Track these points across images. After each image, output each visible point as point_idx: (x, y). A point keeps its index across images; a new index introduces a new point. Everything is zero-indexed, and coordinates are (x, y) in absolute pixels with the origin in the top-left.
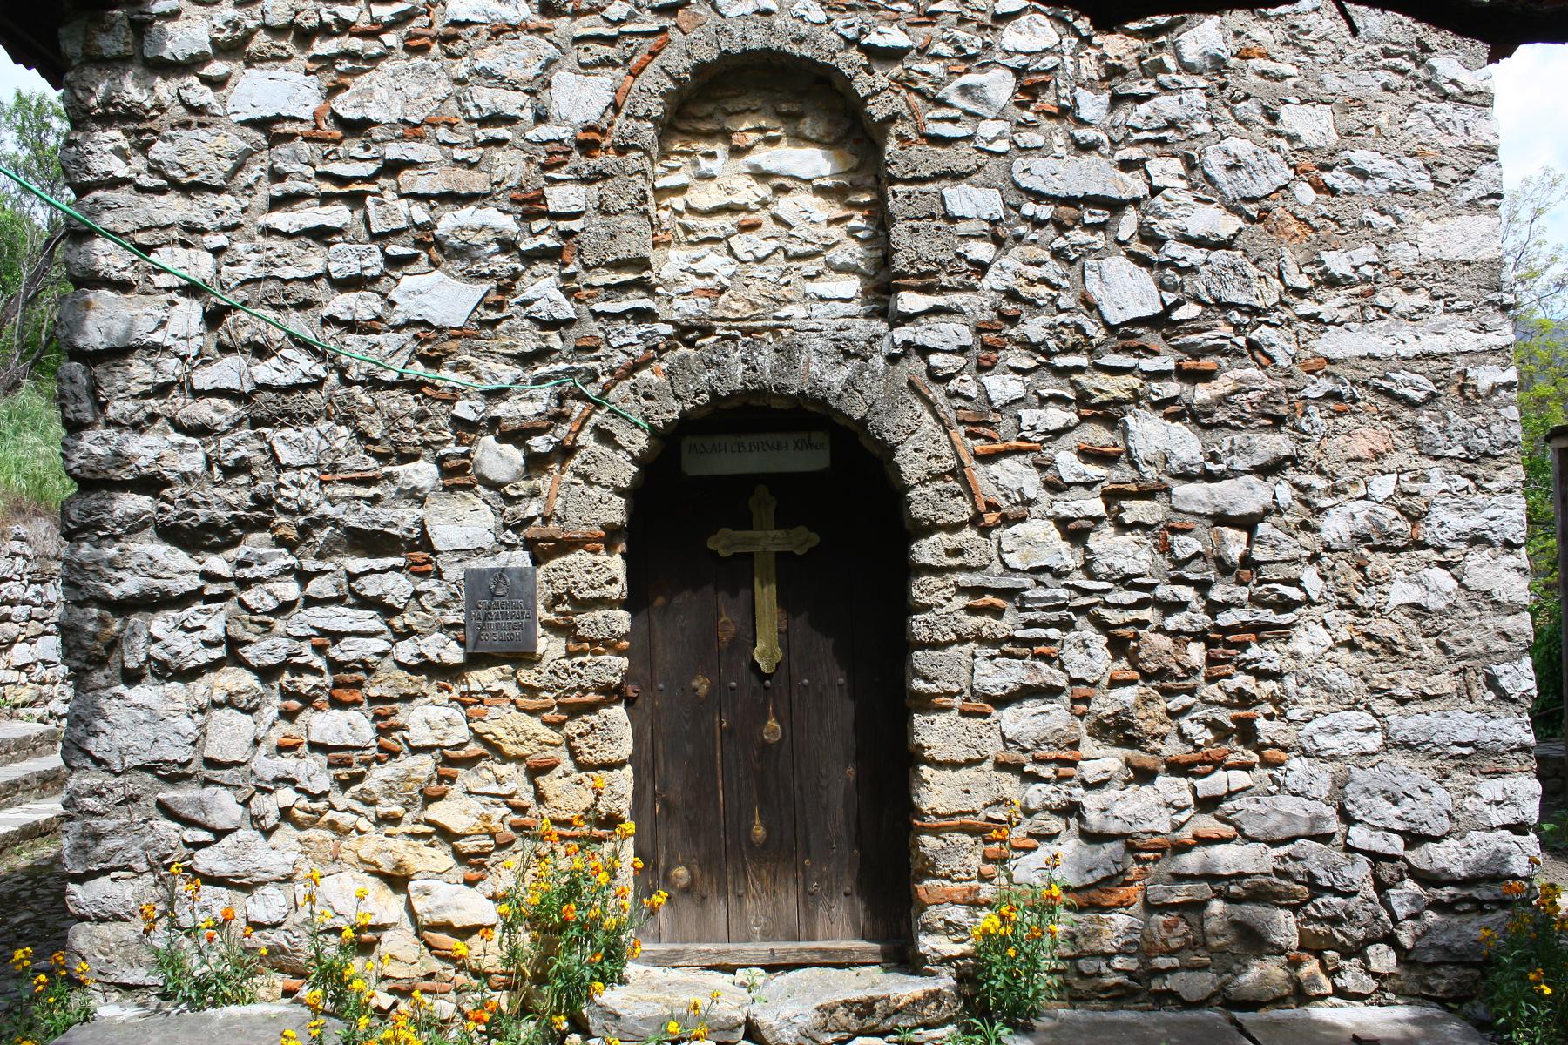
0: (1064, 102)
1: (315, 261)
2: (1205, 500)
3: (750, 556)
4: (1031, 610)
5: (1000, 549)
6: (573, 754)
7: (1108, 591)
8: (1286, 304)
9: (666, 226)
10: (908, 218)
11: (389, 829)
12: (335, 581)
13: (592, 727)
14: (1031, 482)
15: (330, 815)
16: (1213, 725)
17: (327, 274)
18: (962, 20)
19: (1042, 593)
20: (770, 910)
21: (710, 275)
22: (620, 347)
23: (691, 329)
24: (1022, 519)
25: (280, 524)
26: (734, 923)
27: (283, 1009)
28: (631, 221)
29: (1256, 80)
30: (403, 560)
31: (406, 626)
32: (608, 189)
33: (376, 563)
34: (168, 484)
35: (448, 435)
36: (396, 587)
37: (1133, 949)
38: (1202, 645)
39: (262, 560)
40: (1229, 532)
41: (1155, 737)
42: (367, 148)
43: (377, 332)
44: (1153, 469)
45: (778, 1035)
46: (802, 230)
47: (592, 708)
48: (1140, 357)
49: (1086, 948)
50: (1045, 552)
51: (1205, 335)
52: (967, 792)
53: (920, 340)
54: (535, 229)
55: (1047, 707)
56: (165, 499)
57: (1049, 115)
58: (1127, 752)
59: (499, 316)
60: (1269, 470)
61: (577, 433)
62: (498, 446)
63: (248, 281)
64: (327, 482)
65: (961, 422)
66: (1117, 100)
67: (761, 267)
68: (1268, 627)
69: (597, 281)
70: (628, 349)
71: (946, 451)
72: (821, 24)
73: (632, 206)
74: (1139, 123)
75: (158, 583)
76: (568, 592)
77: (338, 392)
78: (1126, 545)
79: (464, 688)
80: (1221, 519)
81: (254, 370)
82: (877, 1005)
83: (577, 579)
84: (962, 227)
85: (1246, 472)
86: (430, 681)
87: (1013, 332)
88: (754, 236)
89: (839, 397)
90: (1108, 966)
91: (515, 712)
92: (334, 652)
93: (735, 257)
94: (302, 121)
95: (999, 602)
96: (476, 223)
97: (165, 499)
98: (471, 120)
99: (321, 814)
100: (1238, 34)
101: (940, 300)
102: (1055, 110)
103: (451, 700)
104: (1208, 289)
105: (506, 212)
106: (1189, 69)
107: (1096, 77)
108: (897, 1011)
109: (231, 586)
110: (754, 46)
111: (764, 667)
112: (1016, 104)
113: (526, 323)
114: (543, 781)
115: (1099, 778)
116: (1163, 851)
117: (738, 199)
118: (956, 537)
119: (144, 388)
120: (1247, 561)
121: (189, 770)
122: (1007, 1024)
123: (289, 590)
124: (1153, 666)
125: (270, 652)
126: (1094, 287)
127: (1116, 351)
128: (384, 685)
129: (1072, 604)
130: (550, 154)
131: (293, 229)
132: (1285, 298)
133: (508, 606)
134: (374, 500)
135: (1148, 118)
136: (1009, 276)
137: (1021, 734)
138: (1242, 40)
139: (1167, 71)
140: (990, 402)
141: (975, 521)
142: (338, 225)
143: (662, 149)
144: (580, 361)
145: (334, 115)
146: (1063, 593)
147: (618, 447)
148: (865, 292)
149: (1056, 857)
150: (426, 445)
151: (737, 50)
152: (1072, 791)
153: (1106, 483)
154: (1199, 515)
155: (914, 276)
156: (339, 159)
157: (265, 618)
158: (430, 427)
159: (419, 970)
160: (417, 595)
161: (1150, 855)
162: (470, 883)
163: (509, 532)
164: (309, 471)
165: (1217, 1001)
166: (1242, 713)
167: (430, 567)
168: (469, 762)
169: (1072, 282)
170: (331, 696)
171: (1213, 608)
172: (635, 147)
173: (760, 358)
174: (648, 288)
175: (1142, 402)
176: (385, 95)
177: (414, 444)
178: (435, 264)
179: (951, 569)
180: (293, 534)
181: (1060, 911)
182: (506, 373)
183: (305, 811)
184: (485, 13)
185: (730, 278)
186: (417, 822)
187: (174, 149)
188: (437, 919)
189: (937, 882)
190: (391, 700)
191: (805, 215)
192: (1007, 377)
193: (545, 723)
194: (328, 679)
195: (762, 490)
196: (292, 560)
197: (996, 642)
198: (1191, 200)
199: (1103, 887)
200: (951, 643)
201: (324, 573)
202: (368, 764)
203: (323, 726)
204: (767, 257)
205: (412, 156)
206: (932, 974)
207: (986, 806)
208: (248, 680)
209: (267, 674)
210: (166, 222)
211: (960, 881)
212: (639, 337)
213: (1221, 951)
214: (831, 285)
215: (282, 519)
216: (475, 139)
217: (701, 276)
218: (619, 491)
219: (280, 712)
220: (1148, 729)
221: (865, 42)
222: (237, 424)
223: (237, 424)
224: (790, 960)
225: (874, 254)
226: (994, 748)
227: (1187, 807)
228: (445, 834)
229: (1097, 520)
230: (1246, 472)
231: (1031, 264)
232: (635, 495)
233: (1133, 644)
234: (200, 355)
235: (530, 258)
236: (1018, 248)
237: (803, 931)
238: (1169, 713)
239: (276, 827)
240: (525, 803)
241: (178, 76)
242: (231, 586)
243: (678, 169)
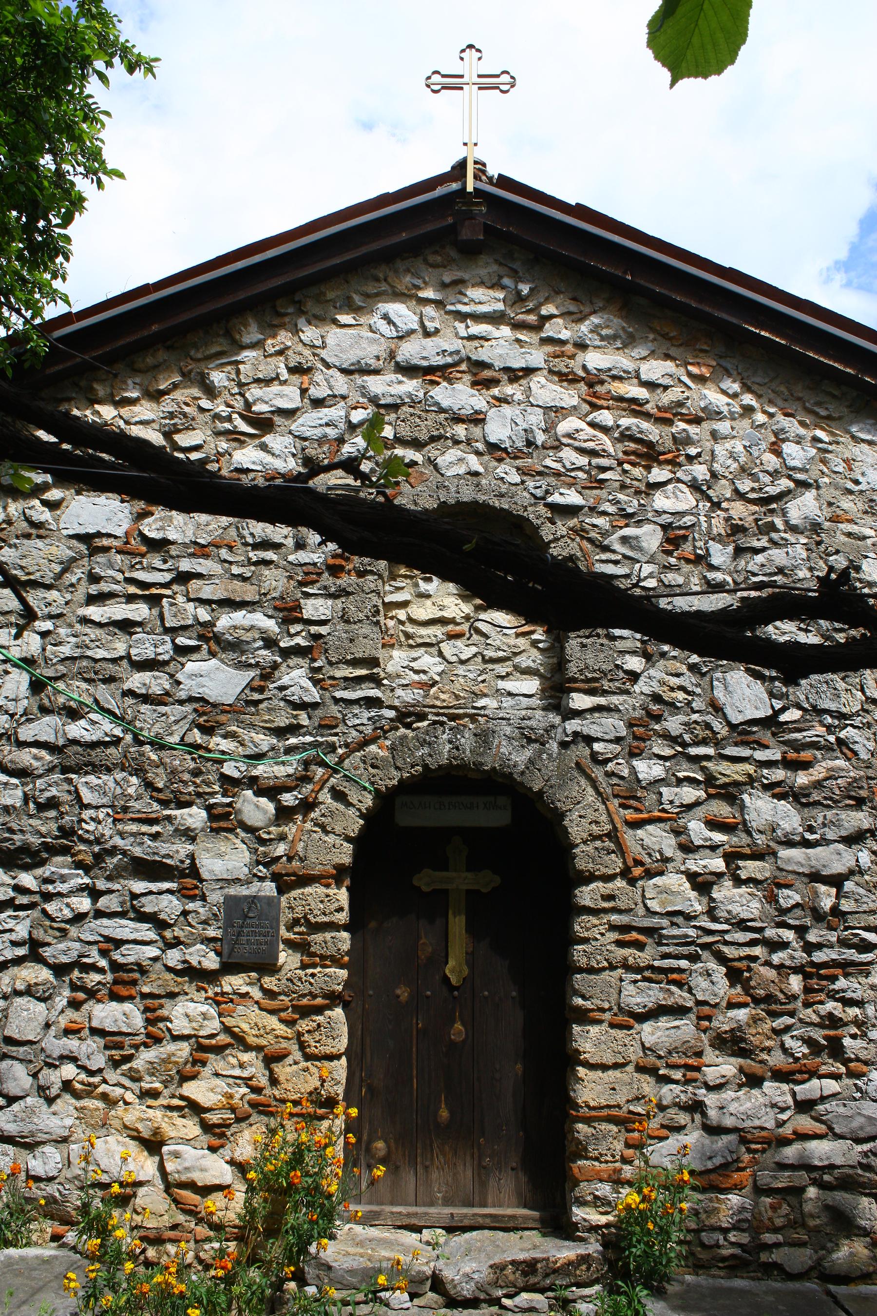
0: (699, 552)
1: (120, 647)
2: (804, 862)
3: (446, 892)
4: (667, 945)
5: (643, 896)
6: (302, 1046)
8: (867, 711)
9: (391, 632)
11: (150, 1102)
12: (121, 899)
13: (319, 1025)
14: (668, 844)
15: (103, 1088)
16: (809, 1042)
17: (128, 656)
18: (623, 487)
19: (675, 932)
20: (450, 1179)
21: (424, 672)
22: (354, 726)
23: (410, 714)
24: (661, 873)
25: (80, 851)
26: (421, 1189)
27: (53, 1252)
28: (366, 629)
29: (844, 539)
30: (175, 885)
31: (175, 938)
32: (350, 604)
33: (154, 886)
35: (217, 788)
37: (745, 1225)
38: (800, 977)
39: (63, 879)
40: (822, 888)
41: (762, 1050)
42: (165, 562)
44: (763, 837)
45: (459, 1288)
46: (496, 639)
47: (319, 1010)
48: (754, 749)
49: (707, 1223)
50: (679, 899)
51: (805, 734)
53: (586, 731)
54: (292, 631)
55: (677, 1023)
57: (688, 561)
58: (740, 1060)
59: (261, 697)
60: (854, 839)
61: (318, 792)
62: (255, 799)
63: (67, 659)
64: (119, 820)
65: (616, 796)
66: (739, 551)
67: (464, 667)
68: (853, 964)
69: (338, 674)
71: (604, 818)
72: (516, 484)
73: (367, 617)
74: (755, 569)
76: (305, 917)
77: (132, 750)
78: (741, 896)
79: (218, 990)
80: (816, 877)
81: (67, 728)
82: (539, 1265)
83: (313, 907)
85: (835, 841)
86: (191, 982)
87: (657, 727)
88: (459, 643)
89: (523, 773)
90: (725, 1239)
91: (258, 1011)
92: (116, 956)
93: (444, 658)
94: (116, 537)
95: (641, 938)
96: (247, 623)
98: (246, 544)
99: (96, 1087)
100: (830, 504)
101: (602, 701)
102: (692, 557)
103: (207, 999)
104: (807, 698)
105: (270, 617)
106: (793, 529)
107: (723, 533)
108: (555, 1271)
109: (37, 898)
110: (465, 500)
111: (454, 981)
112: (663, 551)
113: (282, 704)
114: (277, 1068)
115: (718, 1082)
116: (769, 1143)
117: (447, 614)
118: (610, 885)
120: (835, 910)
122: (646, 1286)
123: (84, 904)
124: (762, 992)
125: (65, 952)
126: (719, 693)
127: (736, 744)
128: (155, 984)
130: (306, 574)
131: (104, 620)
132: (866, 707)
133: (257, 926)
134: (155, 836)
135: (763, 565)
136: (655, 684)
137: (657, 1043)
138: (833, 508)
139: (777, 531)
140: (639, 781)
141: (625, 873)
142: (139, 619)
143: (391, 573)
144: (322, 736)
145: (141, 534)
146: (692, 932)
147: (349, 804)
148: (543, 690)
149: (685, 1147)
150: (199, 795)
151: (452, 501)
152: (697, 1091)
153: (726, 847)
154: (799, 874)
155: (582, 681)
156: (143, 568)
157: (63, 925)
158: (203, 781)
159: (166, 1221)
160: (185, 913)
161: (759, 1146)
162: (213, 1149)
163: (261, 867)
164: (105, 810)
165: (814, 1274)
166: (832, 1033)
167: (197, 892)
168: (219, 1050)
170: (110, 990)
171: (809, 948)
172: (372, 572)
173: (463, 740)
174: (376, 681)
175: (756, 784)
176: (181, 521)
177: (190, 794)
178: (213, 654)
179: (605, 911)
180: (89, 860)
181: (687, 1191)
182: (265, 742)
183: (82, 1083)
184: (262, 463)
185: (440, 674)
186: (173, 1096)
187: (18, 554)
188: (184, 1178)
189: (587, 1163)
190: (159, 997)
192: (652, 762)
193: (281, 1021)
194: (109, 977)
196: (87, 880)
197: (638, 970)
198: (794, 629)
199: (721, 1172)
200: (604, 969)
202: (136, 1047)
203: (103, 1014)
204: (469, 659)
205: (199, 569)
206: (582, 1240)
207: (628, 1101)
208: (45, 974)
209: (60, 970)
210: (6, 609)
211: (607, 1162)
212: (369, 719)
213: (817, 1230)
214: (517, 684)
215: (82, 847)
216: (249, 559)
217: (417, 672)
218: (348, 839)
219: (68, 1002)
220: (758, 1043)
221: (550, 499)
222: (51, 770)
223: (51, 770)
224: (466, 1222)
225: (551, 661)
226: (634, 1054)
227: (788, 1108)
228: (195, 1108)
229: (719, 875)
230: (835, 841)
231: (672, 675)
232: (359, 842)
233: (746, 974)
234: (25, 713)
235: (286, 653)
236: (662, 662)
237: (477, 1199)
238: (774, 1031)
239: (58, 1096)
240: (261, 1085)
241: (24, 500)
242: (37, 898)
243: (402, 588)
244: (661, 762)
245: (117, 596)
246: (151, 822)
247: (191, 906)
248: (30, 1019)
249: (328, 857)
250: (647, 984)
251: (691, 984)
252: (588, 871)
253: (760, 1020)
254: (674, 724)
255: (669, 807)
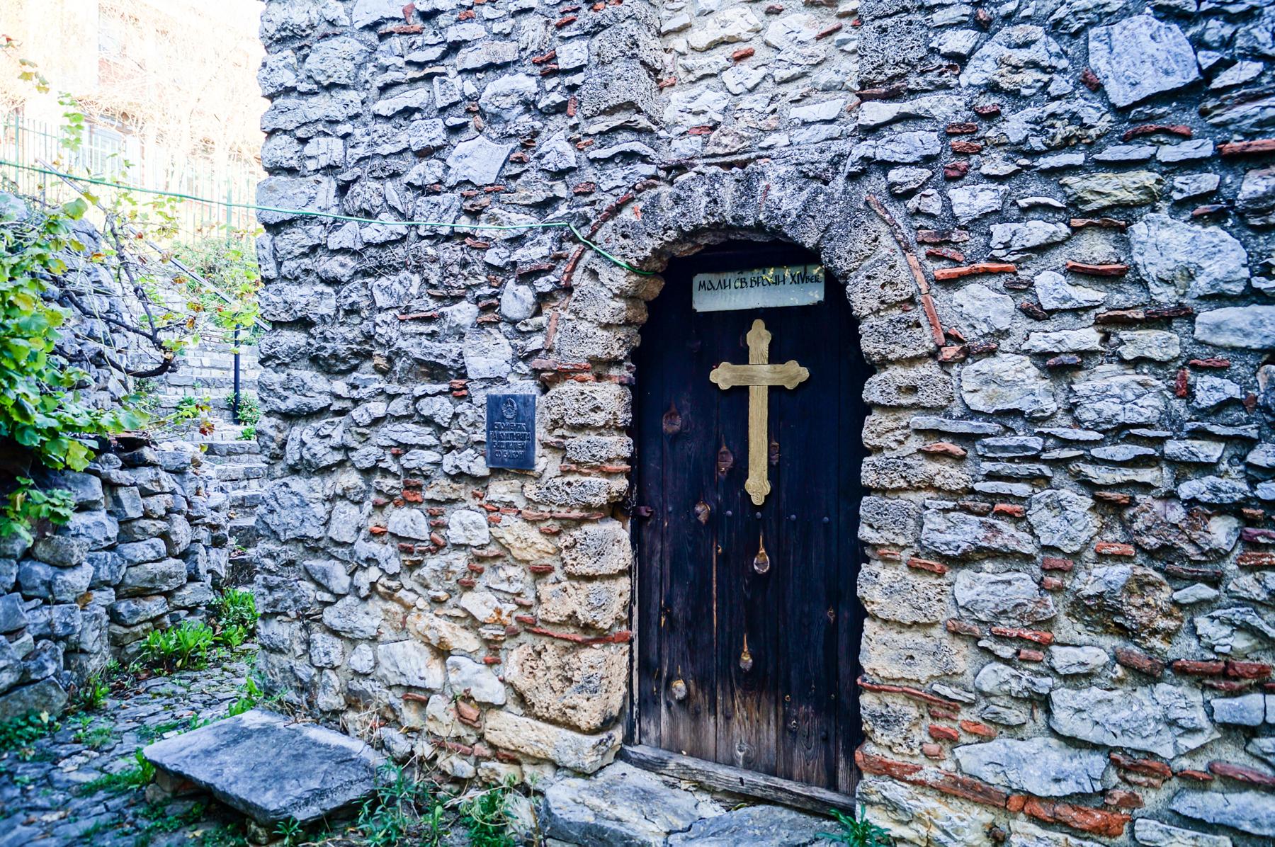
7: (1095, 443)
10: (876, 18)
19: (1007, 441)
21: (704, 112)
24: (992, 353)
34: (313, 324)
35: (483, 279)
36: (441, 408)
38: (1233, 522)
41: (1154, 632)
43: (438, 193)
44: (1171, 291)
50: (1015, 392)
52: (912, 657)
53: (881, 154)
56: (312, 336)
69: (593, 129)
70: (615, 192)
75: (305, 400)
78: (1125, 387)
84: (939, 17)
87: (991, 133)
88: (745, 66)
96: (506, 90)
97: (312, 336)
99: (395, 591)
101: (907, 107)
109: (348, 404)
113: (540, 175)
117: (729, 32)
119: (302, 250)
121: (322, 544)
126: (1099, 61)
127: (1126, 140)
129: (1044, 456)
131: (390, 113)
146: (1036, 443)
150: (468, 287)
167: (464, 392)
169: (1072, 60)
173: (721, 191)
177: (459, 287)
182: (522, 222)
183: (383, 585)
190: (439, 503)
191: (791, 36)
193: (542, 532)
195: (759, 327)
201: (400, 395)
217: (696, 114)
220: (1145, 620)
228: (472, 623)
231: (1019, 46)
242: (348, 404)
244: (993, 186)
245: (401, 84)
246: (428, 320)
247: (459, 409)
248: (346, 522)
249: (581, 349)
250: (962, 515)
251: (1031, 520)
252: (878, 353)
253: (1150, 584)
254: (1015, 126)
255: (1004, 252)
